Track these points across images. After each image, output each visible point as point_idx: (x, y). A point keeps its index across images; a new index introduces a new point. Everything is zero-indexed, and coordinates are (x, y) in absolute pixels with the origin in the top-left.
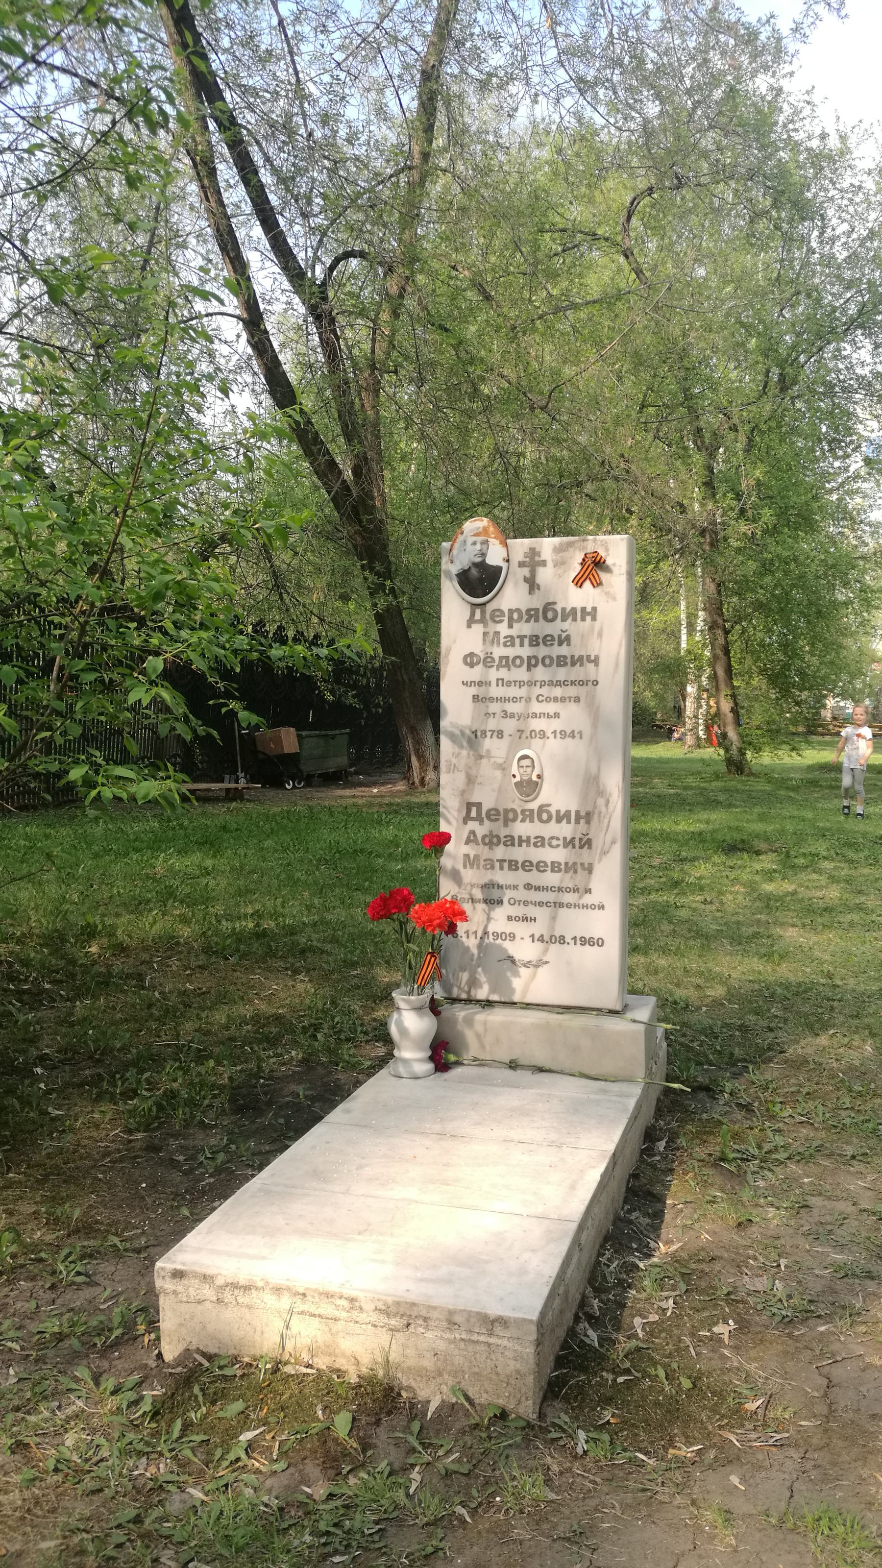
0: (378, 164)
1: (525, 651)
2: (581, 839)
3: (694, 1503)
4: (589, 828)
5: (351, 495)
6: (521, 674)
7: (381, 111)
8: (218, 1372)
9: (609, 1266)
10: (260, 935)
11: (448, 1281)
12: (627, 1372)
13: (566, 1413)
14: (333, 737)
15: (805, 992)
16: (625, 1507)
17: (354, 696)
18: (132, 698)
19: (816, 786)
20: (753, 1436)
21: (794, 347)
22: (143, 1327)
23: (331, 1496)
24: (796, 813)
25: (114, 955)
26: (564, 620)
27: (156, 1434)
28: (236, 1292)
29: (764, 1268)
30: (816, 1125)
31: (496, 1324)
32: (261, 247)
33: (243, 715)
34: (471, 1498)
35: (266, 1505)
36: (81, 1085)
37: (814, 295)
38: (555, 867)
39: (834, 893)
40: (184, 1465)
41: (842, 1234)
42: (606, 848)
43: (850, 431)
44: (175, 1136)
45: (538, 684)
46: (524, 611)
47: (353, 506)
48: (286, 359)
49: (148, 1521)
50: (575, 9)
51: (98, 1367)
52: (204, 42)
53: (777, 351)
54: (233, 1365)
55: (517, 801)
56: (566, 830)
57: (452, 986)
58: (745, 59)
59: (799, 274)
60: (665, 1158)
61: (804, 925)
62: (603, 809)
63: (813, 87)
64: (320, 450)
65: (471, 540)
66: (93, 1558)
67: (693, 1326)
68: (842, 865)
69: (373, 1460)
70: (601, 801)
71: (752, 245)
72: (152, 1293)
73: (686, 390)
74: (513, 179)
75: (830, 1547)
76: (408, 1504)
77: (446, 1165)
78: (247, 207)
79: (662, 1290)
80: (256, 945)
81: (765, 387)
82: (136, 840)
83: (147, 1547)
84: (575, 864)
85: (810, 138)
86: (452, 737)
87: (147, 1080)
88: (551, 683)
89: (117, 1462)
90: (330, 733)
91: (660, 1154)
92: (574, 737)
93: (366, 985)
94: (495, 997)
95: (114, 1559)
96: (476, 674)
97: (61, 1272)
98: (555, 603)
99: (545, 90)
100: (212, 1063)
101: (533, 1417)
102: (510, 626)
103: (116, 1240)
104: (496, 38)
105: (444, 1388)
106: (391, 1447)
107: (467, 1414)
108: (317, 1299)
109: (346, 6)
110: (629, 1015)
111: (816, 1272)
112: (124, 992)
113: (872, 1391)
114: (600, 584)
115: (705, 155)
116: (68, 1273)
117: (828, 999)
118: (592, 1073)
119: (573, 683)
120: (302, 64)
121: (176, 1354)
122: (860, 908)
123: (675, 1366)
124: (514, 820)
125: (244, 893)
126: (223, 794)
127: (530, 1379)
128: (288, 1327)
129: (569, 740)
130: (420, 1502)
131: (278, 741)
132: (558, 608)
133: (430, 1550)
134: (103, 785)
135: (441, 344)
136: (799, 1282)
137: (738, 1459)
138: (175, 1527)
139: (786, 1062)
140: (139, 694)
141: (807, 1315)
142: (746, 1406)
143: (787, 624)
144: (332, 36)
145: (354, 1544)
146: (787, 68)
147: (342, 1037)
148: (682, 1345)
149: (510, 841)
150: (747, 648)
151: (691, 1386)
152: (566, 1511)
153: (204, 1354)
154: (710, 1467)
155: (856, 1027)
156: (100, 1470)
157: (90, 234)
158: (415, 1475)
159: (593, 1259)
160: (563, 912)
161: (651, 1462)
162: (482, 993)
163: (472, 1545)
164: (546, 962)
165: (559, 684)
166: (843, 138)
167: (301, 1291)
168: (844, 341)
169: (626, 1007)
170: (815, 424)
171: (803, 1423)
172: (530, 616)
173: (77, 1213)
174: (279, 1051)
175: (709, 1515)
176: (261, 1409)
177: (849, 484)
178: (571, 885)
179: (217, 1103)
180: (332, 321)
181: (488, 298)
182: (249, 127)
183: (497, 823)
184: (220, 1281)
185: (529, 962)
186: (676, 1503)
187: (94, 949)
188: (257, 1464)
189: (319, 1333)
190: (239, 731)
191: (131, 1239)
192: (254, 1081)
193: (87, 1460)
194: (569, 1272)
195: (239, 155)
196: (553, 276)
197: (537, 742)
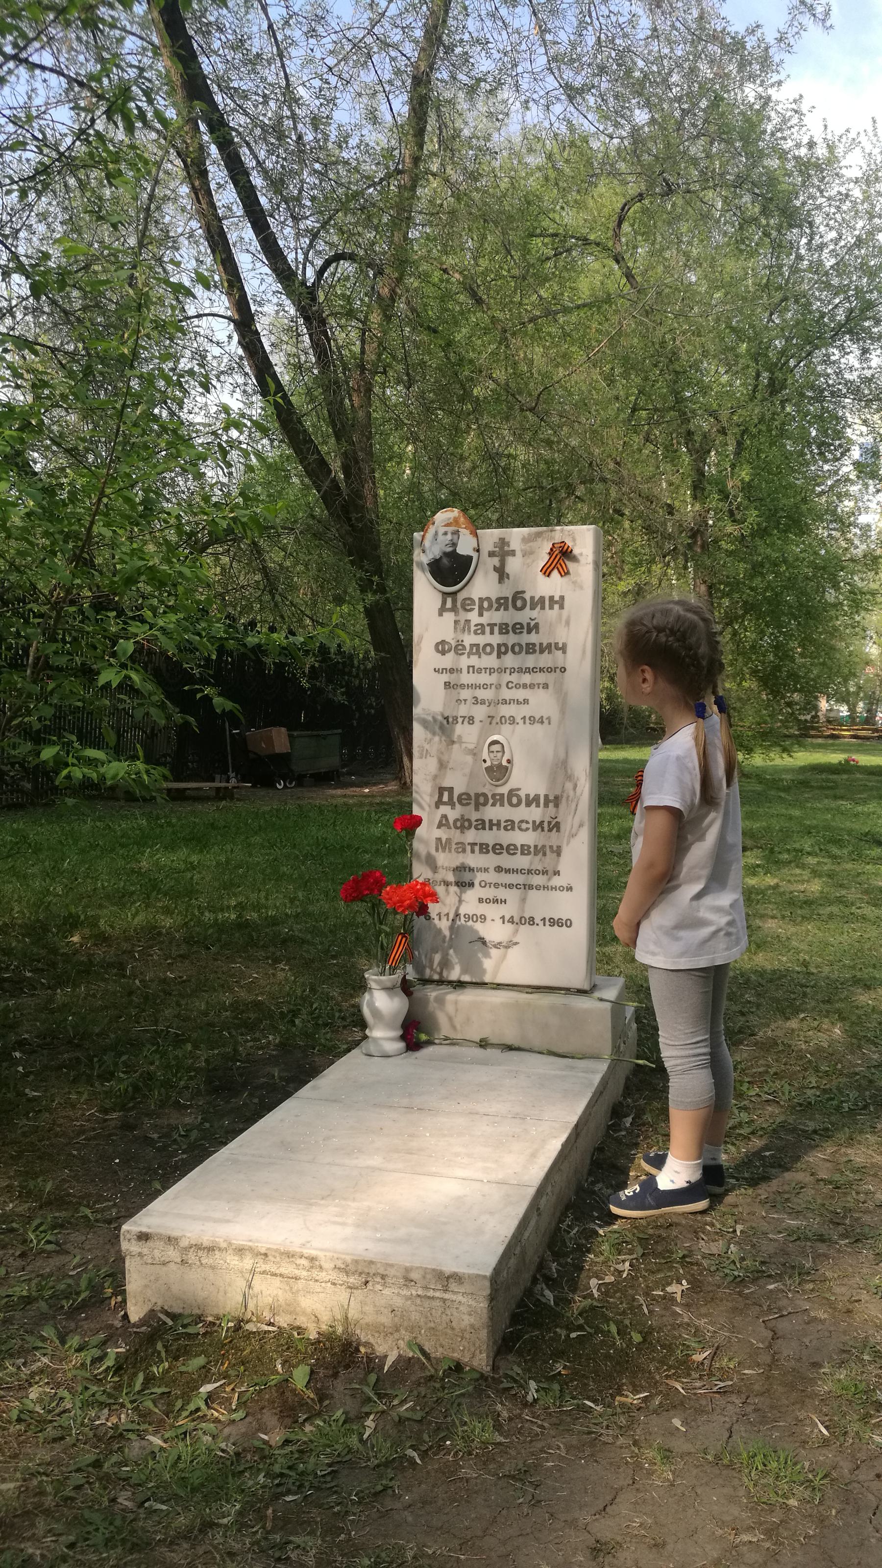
0: (368, 167)
1: (496, 639)
2: (549, 823)
3: (635, 1443)
4: (557, 812)
5: (340, 494)
6: (491, 661)
7: (373, 117)
8: (181, 1330)
9: (569, 1232)
10: (242, 925)
11: (407, 1241)
12: (580, 1328)
13: (519, 1365)
14: (325, 737)
15: (779, 979)
16: (569, 1448)
17: (342, 694)
18: (102, 680)
19: (807, 787)
20: (698, 1384)
21: (783, 352)
22: (110, 1290)
23: (287, 1442)
24: (784, 811)
25: (96, 945)
26: (532, 608)
27: (118, 1387)
28: (200, 1253)
29: (720, 1234)
30: (782, 1103)
31: (451, 1280)
32: (252, 249)
33: (217, 700)
34: (423, 1442)
35: (223, 1451)
36: (60, 1068)
37: (803, 301)
38: (525, 850)
39: (815, 887)
40: (144, 1416)
41: (799, 1202)
42: (574, 831)
43: (839, 435)
44: (149, 1115)
45: (508, 671)
46: (494, 600)
47: (343, 506)
48: (277, 359)
49: (106, 1465)
50: (564, 17)
51: (64, 1327)
52: (195, 46)
53: (766, 356)
54: (196, 1324)
55: (488, 786)
56: (535, 814)
57: (424, 967)
58: (732, 68)
59: (787, 281)
60: (630, 1132)
61: (783, 917)
62: (571, 793)
63: (801, 96)
64: (309, 449)
65: (442, 530)
66: (50, 1498)
67: (647, 1287)
68: (825, 860)
69: (330, 1409)
70: (569, 786)
71: (741, 251)
72: (120, 1259)
73: (677, 393)
74: (504, 184)
75: (762, 1481)
76: (361, 1448)
77: (412, 1136)
78: (239, 210)
79: (619, 1254)
80: (237, 935)
81: (754, 391)
82: (122, 837)
83: (105, 1488)
84: (544, 846)
85: (798, 146)
86: (425, 723)
87: (124, 1063)
88: (520, 670)
89: (79, 1412)
90: (321, 733)
91: (626, 1129)
92: (542, 722)
93: (345, 973)
94: (466, 978)
95: (72, 1499)
96: (448, 660)
97: (31, 1241)
98: (524, 592)
99: (535, 96)
100: (189, 1047)
101: (486, 1369)
102: (481, 614)
103: (88, 1212)
104: (483, 43)
105: (401, 1343)
106: (347, 1397)
107: (423, 1367)
108: (278, 1259)
109: (336, 11)
110: (597, 994)
111: (770, 1236)
112: (104, 980)
113: (815, 1342)
114: (567, 573)
115: (695, 161)
116: (39, 1242)
117: (802, 986)
118: (560, 1051)
119: (541, 670)
120: (292, 66)
121: (142, 1315)
122: (840, 900)
123: (627, 1322)
124: (485, 804)
125: (229, 886)
126: (213, 793)
127: (484, 1334)
128: (250, 1287)
129: (537, 726)
130: (373, 1446)
131: (270, 741)
132: (527, 597)
133: (379, 1488)
134: (73, 765)
135: (430, 345)
136: (753, 1246)
137: (682, 1404)
138: (133, 1471)
139: (755, 1044)
140: (109, 676)
141: (759, 1276)
142: (694, 1357)
143: (779, 627)
144: (324, 41)
145: (307, 1484)
146: (775, 78)
147: (320, 1022)
148: (635, 1304)
149: (482, 825)
150: (740, 651)
151: (641, 1339)
152: (513, 1452)
153: (167, 1314)
154: (655, 1412)
155: (828, 1012)
156: (64, 1421)
157: (80, 234)
158: (370, 1423)
159: (553, 1225)
160: (533, 893)
161: (598, 1408)
162: (455, 974)
163: (420, 1484)
164: (516, 943)
165: (528, 670)
166: (831, 148)
167: (263, 1251)
168: (833, 347)
169: (594, 988)
170: (804, 428)
171: (746, 1372)
172: (500, 605)
173: (49, 1186)
174: (257, 1035)
175: (650, 1453)
176: (223, 1364)
177: (838, 487)
178: (540, 868)
179: (192, 1083)
180: (323, 322)
181: (479, 301)
182: (241, 129)
183: (468, 807)
184: (184, 1243)
185: (500, 943)
186: (618, 1443)
187: (76, 939)
188: (216, 1414)
189: (280, 1292)
190: (230, 731)
191: (103, 1210)
192: (230, 1064)
193: (50, 1412)
194: (527, 1234)
195: (229, 155)
196: (543, 280)
197: (506, 728)
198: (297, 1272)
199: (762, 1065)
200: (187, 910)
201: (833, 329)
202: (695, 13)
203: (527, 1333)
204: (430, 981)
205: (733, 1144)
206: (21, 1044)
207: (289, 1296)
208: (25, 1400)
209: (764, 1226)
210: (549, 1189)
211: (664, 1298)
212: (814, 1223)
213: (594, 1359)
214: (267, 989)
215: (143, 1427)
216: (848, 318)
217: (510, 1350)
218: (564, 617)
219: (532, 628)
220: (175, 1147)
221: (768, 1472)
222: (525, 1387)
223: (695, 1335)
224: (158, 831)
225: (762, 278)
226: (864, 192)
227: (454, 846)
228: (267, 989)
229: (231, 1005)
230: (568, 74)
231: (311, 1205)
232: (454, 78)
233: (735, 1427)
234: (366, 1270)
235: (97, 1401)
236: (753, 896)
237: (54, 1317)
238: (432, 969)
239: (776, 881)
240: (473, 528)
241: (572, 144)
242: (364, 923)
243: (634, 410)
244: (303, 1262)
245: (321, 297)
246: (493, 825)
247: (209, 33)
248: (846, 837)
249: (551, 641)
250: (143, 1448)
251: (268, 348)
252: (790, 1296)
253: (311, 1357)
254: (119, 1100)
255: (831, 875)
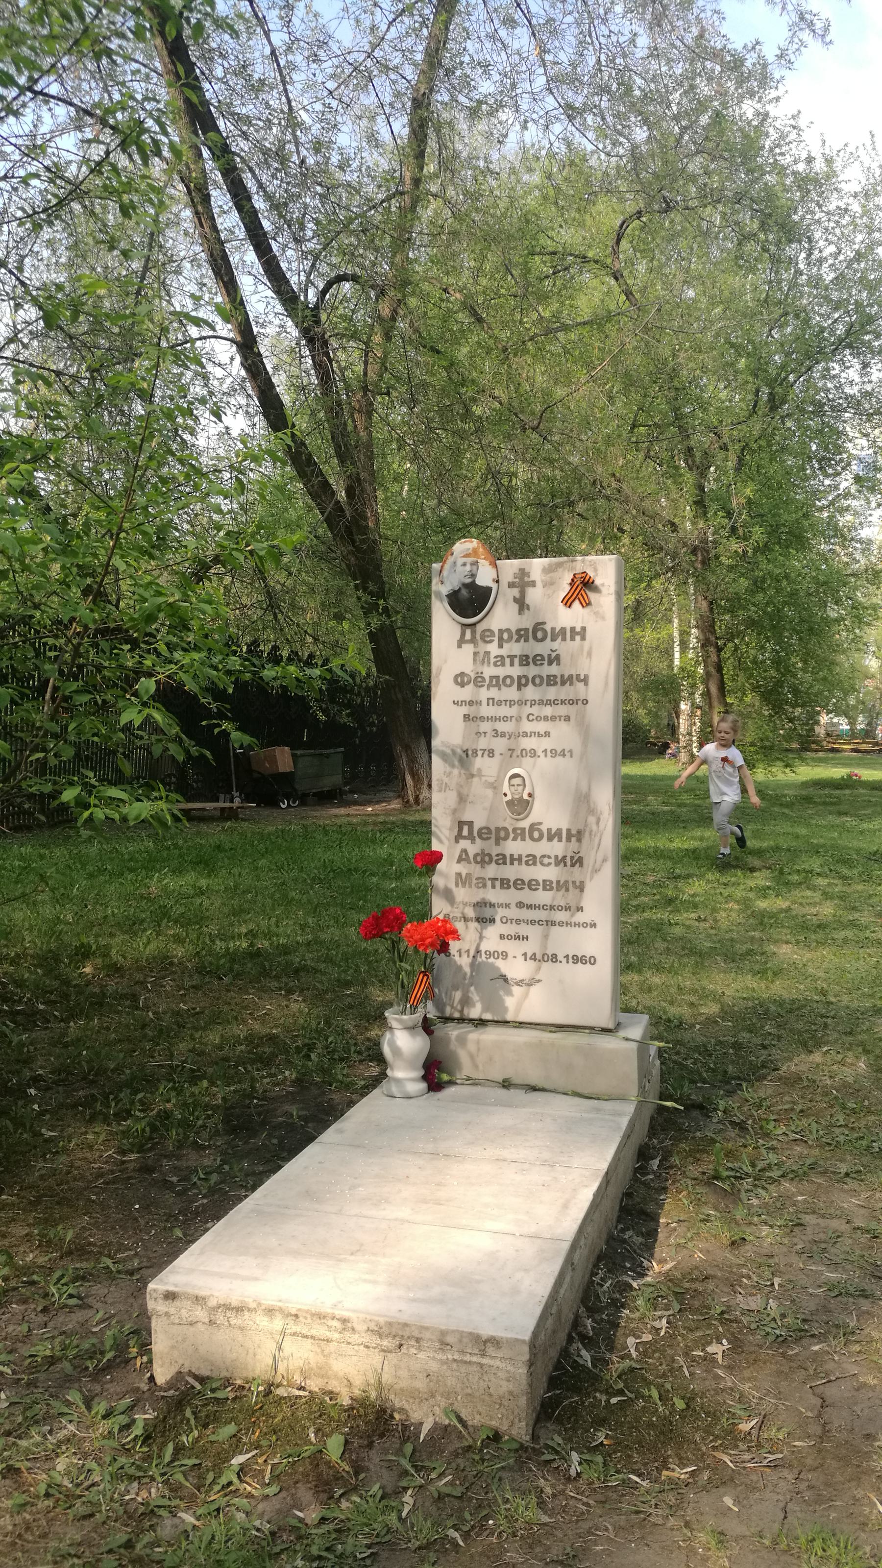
0: (370, 189)
1: (516, 671)
2: (572, 858)
3: (687, 1525)
4: (580, 846)
5: (344, 516)
6: (511, 693)
7: (372, 139)
8: (210, 1395)
9: (602, 1286)
10: (255, 955)
11: (441, 1301)
12: (621, 1392)
13: (560, 1434)
14: (328, 756)
15: (798, 1009)
16: (618, 1529)
17: (348, 715)
18: (124, 719)
19: (809, 803)
20: (747, 1457)
21: (783, 367)
22: (135, 1350)
23: (323, 1520)
24: (790, 830)
25: (108, 976)
27: (148, 1458)
28: (229, 1314)
29: (758, 1287)
30: (810, 1142)
31: (489, 1344)
32: (254, 271)
33: (236, 735)
35: (258, 1530)
36: (74, 1106)
37: (802, 316)
38: (547, 885)
39: (827, 910)
40: (175, 1489)
41: (836, 1252)
43: (839, 449)
45: (529, 703)
46: (514, 631)
48: (280, 381)
49: (139, 1546)
50: (563, 38)
53: (766, 371)
54: (226, 1387)
55: (509, 819)
56: (557, 848)
57: (444, 1005)
58: (731, 85)
59: (787, 295)
61: (798, 942)
62: (594, 828)
63: (799, 112)
65: (460, 561)
67: (686, 1346)
70: (592, 820)
71: (740, 267)
72: (145, 1316)
73: (676, 410)
76: (401, 1529)
77: (439, 1184)
78: (241, 233)
79: (655, 1310)
80: (249, 965)
82: (131, 860)
84: (566, 882)
85: (796, 162)
86: (444, 756)
87: (140, 1100)
88: (541, 702)
89: (108, 1486)
90: (324, 752)
91: (654, 1172)
92: (564, 755)
93: (360, 1004)
94: (488, 1016)
96: (466, 693)
97: (53, 1295)
98: (544, 623)
99: (535, 116)
100: (205, 1083)
102: (500, 646)
103: (109, 1262)
104: (485, 67)
105: (437, 1410)
106: (384, 1470)
107: (460, 1436)
108: (309, 1320)
110: (622, 1033)
111: (810, 1290)
112: (118, 1012)
113: (866, 1411)
114: (589, 604)
115: (693, 178)
117: (822, 1016)
118: (585, 1092)
119: (563, 702)
120: (295, 92)
121: (168, 1377)
122: (853, 924)
123: (668, 1386)
124: (506, 838)
125: (238, 912)
126: (218, 813)
127: (523, 1401)
128: (280, 1349)
129: (559, 759)
131: (274, 761)
132: (548, 628)
134: (95, 806)
135: (433, 366)
138: (166, 1552)
139: (780, 1079)
140: (132, 716)
141: (801, 1335)
142: (740, 1426)
144: (324, 65)
146: (773, 94)
147: (336, 1057)
148: (676, 1365)
149: (502, 860)
150: (740, 664)
151: (684, 1406)
152: (559, 1534)
153: (196, 1377)
154: (704, 1488)
155: (850, 1044)
156: (91, 1495)
158: (408, 1498)
160: (555, 930)
161: (644, 1483)
162: (475, 1012)
164: (539, 981)
165: (549, 703)
166: (829, 161)
167: (294, 1312)
168: (833, 361)
169: (618, 1026)
170: (805, 443)
171: (796, 1443)
173: (70, 1235)
174: (273, 1070)
175: (702, 1537)
176: (254, 1433)
180: (325, 343)
181: (480, 320)
182: (243, 154)
184: (212, 1303)
185: (522, 981)
186: (669, 1525)
187: (88, 970)
188: (249, 1488)
189: (311, 1355)
191: (124, 1260)
192: (247, 1102)
193: (78, 1485)
194: (562, 1291)
195: (232, 182)
196: (543, 298)
197: (527, 761)
198: (328, 1333)
199: (788, 1102)
200: (198, 939)
201: (833, 344)
202: (695, 31)
203: (567, 1398)
204: (450, 1019)
205: (764, 1188)
206: (36, 1080)
207: (321, 1359)
208: (52, 1473)
209: (803, 1280)
210: (582, 1243)
211: (705, 1359)
212: (853, 1277)
213: (636, 1428)
214: (281, 1021)
215: (175, 1502)
216: (848, 333)
217: (549, 1417)
218: (586, 649)
219: (554, 659)
220: (196, 1191)
221: (828, 1558)
222: (566, 1459)
223: (740, 1401)
224: (165, 854)
225: (761, 293)
226: (864, 206)
227: (474, 881)
228: (281, 1021)
229: (246, 1038)
230: (570, 95)
231: (340, 1261)
232: (453, 99)
233: (790, 1506)
234: (400, 1333)
235: (126, 1474)
236: (766, 920)
237: (80, 1380)
238: (452, 1007)
239: (787, 904)
240: (492, 560)
241: (572, 163)
242: (376, 951)
243: (634, 426)
244: (335, 1323)
245: (323, 317)
246: (514, 860)
247: (212, 59)
248: (855, 856)
249: (574, 673)
250: (176, 1526)
251: (270, 371)
252: (836, 1358)
253: (345, 1425)
254: (136, 1141)
255: (842, 897)
